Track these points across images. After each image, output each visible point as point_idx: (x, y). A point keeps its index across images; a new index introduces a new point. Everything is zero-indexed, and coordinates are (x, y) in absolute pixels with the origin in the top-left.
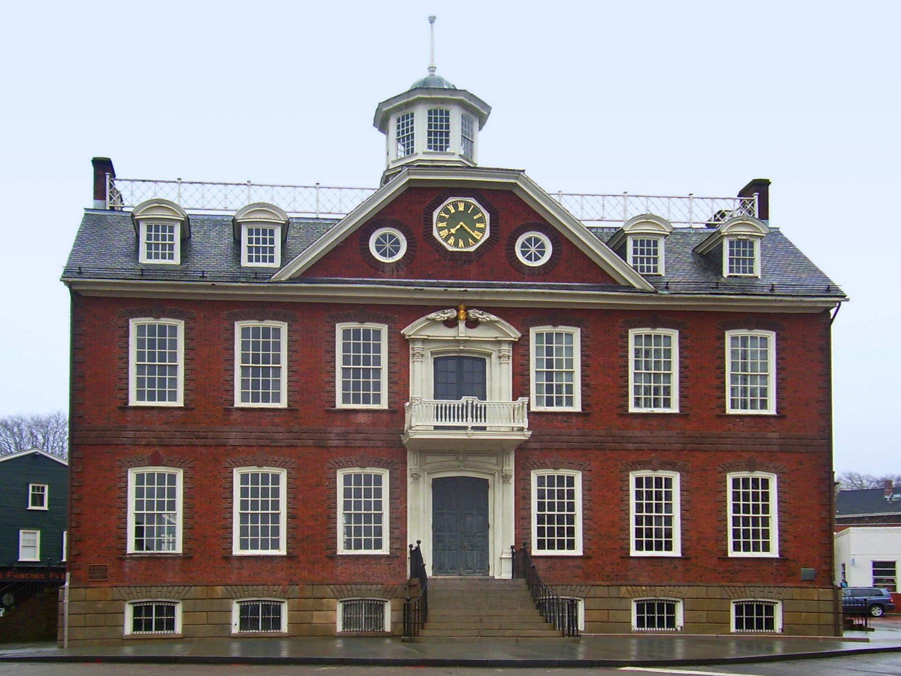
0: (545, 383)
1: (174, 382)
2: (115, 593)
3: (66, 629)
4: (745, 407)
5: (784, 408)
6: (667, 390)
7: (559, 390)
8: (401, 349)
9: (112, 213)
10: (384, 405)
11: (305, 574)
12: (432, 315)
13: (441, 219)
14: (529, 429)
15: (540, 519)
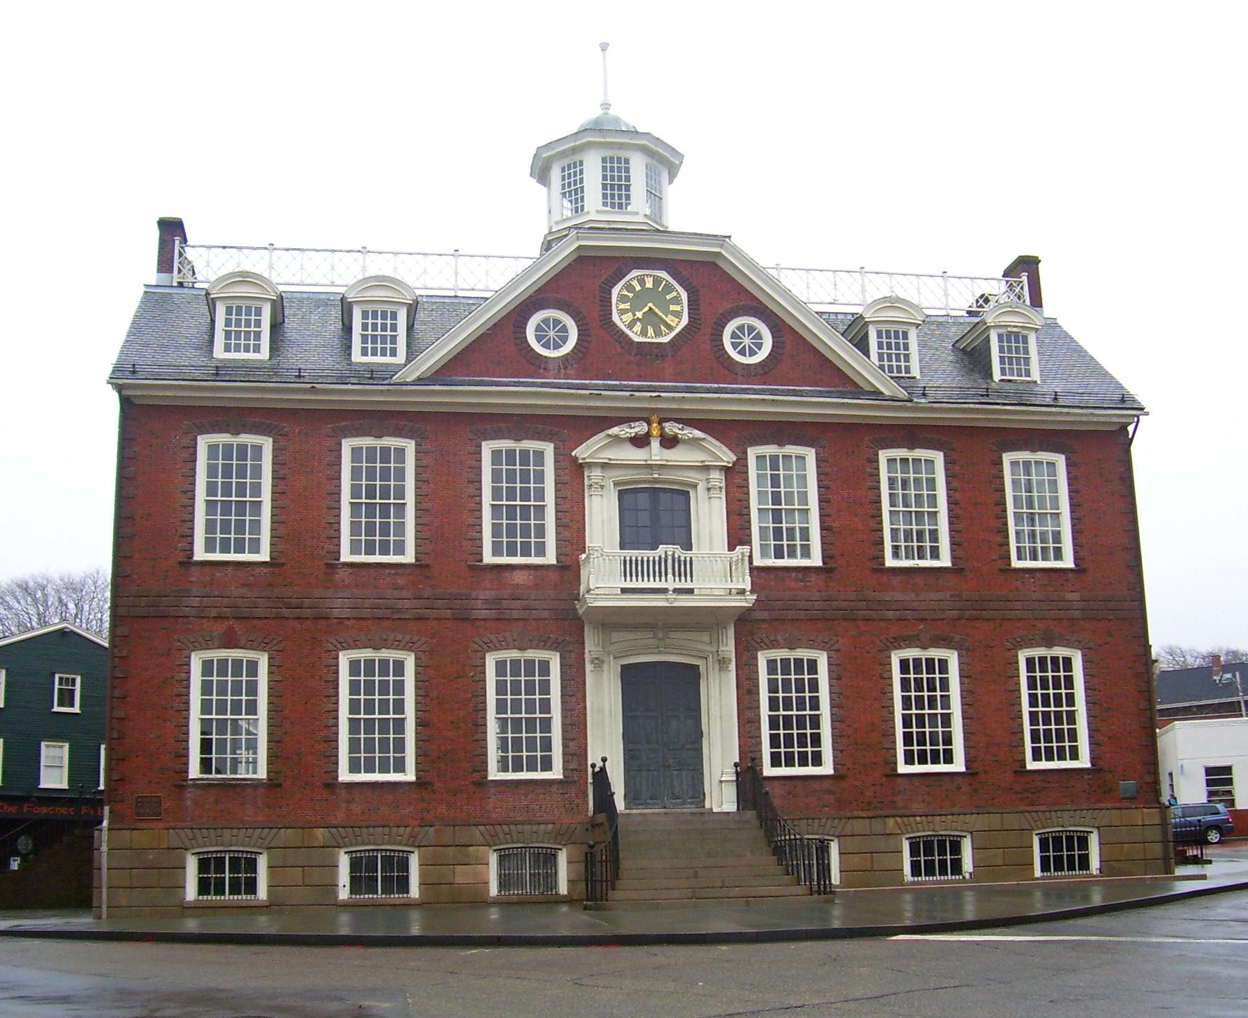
0: (771, 525)
1: (256, 526)
2: (172, 838)
3: (104, 890)
4: (1035, 558)
5: (1083, 559)
6: (934, 535)
7: (791, 537)
8: (573, 476)
9: (180, 291)
10: (551, 558)
11: (442, 809)
12: (615, 431)
13: (622, 299)
14: (752, 591)
15: (774, 723)
